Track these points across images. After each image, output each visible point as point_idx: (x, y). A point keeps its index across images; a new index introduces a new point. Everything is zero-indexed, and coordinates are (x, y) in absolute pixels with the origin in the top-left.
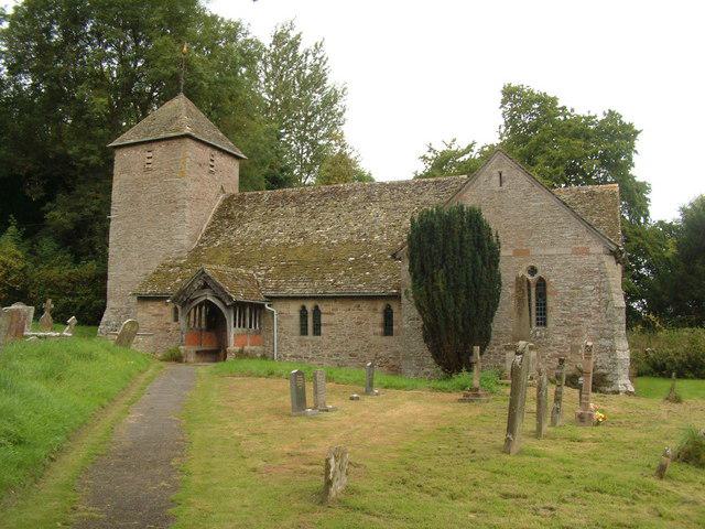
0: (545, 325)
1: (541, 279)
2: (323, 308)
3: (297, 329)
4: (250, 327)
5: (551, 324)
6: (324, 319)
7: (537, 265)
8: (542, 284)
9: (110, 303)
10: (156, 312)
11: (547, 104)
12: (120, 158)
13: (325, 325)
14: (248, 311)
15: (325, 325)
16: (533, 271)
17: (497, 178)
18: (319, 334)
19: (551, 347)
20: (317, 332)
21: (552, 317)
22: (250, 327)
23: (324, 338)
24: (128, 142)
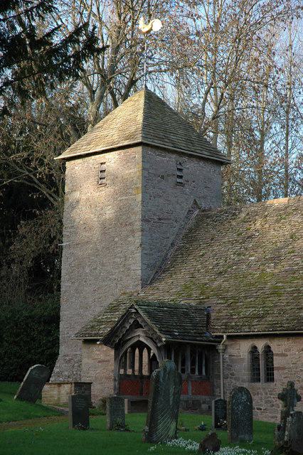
4: (193, 371)
6: (277, 362)
9: (63, 350)
13: (279, 369)
14: (188, 353)
22: (193, 371)
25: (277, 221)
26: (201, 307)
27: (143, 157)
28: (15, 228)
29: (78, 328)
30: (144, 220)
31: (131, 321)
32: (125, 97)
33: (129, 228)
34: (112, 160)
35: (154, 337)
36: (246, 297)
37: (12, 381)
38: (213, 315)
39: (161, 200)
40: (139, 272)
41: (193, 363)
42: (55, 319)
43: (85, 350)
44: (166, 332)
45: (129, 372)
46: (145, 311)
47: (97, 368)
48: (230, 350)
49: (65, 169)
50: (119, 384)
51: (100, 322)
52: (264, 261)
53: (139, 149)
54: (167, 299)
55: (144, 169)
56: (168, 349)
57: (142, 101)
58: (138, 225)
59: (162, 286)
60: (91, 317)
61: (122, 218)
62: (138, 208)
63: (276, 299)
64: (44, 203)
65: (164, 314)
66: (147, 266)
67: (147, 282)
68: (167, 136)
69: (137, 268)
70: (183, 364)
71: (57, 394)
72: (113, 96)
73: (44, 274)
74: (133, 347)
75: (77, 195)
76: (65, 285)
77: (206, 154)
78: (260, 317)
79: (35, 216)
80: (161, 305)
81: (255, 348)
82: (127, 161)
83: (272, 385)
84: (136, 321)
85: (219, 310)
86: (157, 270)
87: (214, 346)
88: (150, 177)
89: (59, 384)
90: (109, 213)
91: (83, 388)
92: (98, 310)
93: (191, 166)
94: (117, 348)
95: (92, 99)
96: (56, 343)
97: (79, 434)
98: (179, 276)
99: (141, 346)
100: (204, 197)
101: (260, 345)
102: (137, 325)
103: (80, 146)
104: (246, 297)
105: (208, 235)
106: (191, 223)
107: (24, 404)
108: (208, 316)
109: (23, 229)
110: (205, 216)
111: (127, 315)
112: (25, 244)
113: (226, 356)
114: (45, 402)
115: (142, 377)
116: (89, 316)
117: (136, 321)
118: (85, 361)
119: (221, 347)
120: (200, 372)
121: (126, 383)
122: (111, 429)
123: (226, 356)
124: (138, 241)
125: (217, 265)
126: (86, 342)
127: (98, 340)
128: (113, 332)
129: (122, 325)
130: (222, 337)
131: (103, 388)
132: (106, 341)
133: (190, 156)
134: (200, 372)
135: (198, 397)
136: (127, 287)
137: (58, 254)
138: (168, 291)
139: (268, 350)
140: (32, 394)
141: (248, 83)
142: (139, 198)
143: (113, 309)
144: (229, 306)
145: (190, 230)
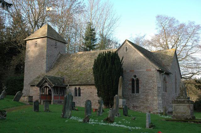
0: (139, 93)
1: (137, 79)
2: (82, 87)
3: (131, 91)
4: (60, 93)
5: (140, 93)
6: (82, 91)
7: (136, 75)
8: (138, 80)
9: (24, 88)
10: (35, 90)
11: (172, 20)
12: (29, 43)
13: (130, 89)
14: (59, 88)
15: (130, 89)
16: (135, 76)
17: (125, 49)
18: (80, 96)
19: (140, 99)
20: (80, 95)
21: (140, 90)
22: (60, 93)
23: (81, 97)
24: (30, 39)
25: (80, 57)
26: (62, 77)
27: (47, 40)
28: (12, 58)
29: (29, 82)
30: (47, 56)
31: (44, 81)
32: (41, 27)
33: (43, 58)
34: (39, 41)
35: (51, 85)
36: (73, 75)
37: (10, 95)
38: (65, 80)
39: (51, 51)
40: (45, 69)
41: (60, 92)
42: (22, 80)
43: (31, 88)
44: (54, 84)
45: (43, 93)
46: (49, 79)
47: (35, 92)
48: (70, 88)
49: (26, 42)
50: (41, 96)
51: (35, 81)
52: (78, 67)
53: (46, 38)
54: (53, 75)
55: (47, 43)
56: (54, 88)
57: (47, 27)
58: (45, 57)
59: (51, 72)
60: (32, 80)
61: (40, 55)
62: (45, 53)
63: (81, 76)
64: (19, 52)
65: (53, 79)
66: (47, 67)
67: (47, 71)
68: (51, 35)
69: (45, 68)
70: (58, 92)
71: (24, 99)
72: (38, 27)
73: (20, 69)
74: (44, 87)
75: (29, 49)
76: (25, 71)
77: (62, 41)
78: (78, 80)
79: (17, 55)
80: (52, 77)
81: (76, 88)
82: (43, 41)
83: (80, 97)
84: (46, 81)
85: (67, 79)
86: (50, 68)
87: (66, 88)
88: (49, 45)
89: (24, 96)
90: (37, 53)
91: (30, 97)
92: (34, 78)
93: (59, 43)
94: (40, 87)
95: (32, 28)
96: (23, 86)
97: (37, 114)
98: (55, 70)
99: (46, 87)
100: (61, 51)
101: (77, 87)
102: (46, 82)
103: (31, 37)
104: (73, 75)
105: (63, 60)
106: (58, 57)
107: (16, 102)
108: (64, 80)
109: (14, 58)
110: (62, 55)
111: (44, 79)
112: (15, 61)
113: (68, 90)
114: (76, 108)
115: (46, 95)
116: (32, 79)
117: (46, 81)
118: (31, 90)
119: (67, 88)
120: (62, 94)
121: (42, 97)
122: (45, 111)
123: (68, 90)
124: (45, 61)
125: (65, 67)
126: (31, 86)
127: (35, 86)
128: (39, 83)
129: (42, 82)
130: (68, 85)
131: (36, 97)
132: (38, 86)
133: (59, 41)
134: (62, 94)
135: (61, 100)
136: (42, 72)
137: (23, 65)
138: (52, 74)
139: (79, 88)
140: (17, 99)
141: (70, 27)
142: (46, 50)
143: (38, 78)
144: (69, 77)
145: (58, 59)
